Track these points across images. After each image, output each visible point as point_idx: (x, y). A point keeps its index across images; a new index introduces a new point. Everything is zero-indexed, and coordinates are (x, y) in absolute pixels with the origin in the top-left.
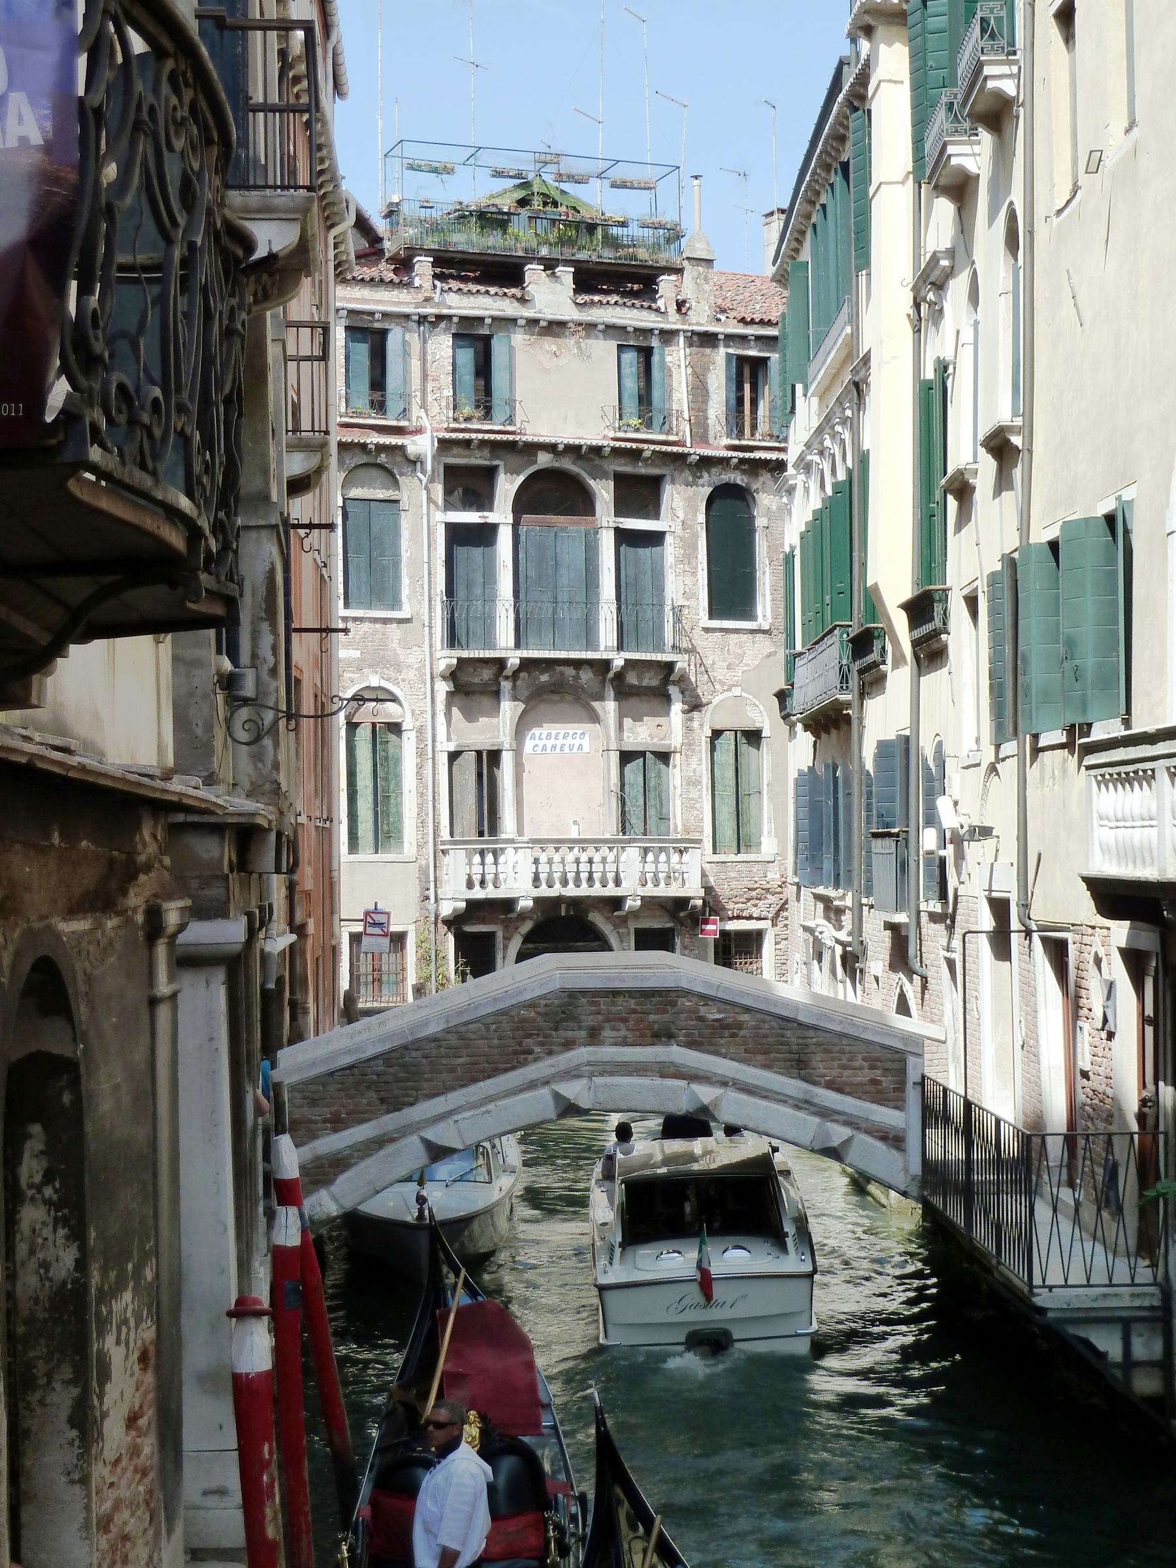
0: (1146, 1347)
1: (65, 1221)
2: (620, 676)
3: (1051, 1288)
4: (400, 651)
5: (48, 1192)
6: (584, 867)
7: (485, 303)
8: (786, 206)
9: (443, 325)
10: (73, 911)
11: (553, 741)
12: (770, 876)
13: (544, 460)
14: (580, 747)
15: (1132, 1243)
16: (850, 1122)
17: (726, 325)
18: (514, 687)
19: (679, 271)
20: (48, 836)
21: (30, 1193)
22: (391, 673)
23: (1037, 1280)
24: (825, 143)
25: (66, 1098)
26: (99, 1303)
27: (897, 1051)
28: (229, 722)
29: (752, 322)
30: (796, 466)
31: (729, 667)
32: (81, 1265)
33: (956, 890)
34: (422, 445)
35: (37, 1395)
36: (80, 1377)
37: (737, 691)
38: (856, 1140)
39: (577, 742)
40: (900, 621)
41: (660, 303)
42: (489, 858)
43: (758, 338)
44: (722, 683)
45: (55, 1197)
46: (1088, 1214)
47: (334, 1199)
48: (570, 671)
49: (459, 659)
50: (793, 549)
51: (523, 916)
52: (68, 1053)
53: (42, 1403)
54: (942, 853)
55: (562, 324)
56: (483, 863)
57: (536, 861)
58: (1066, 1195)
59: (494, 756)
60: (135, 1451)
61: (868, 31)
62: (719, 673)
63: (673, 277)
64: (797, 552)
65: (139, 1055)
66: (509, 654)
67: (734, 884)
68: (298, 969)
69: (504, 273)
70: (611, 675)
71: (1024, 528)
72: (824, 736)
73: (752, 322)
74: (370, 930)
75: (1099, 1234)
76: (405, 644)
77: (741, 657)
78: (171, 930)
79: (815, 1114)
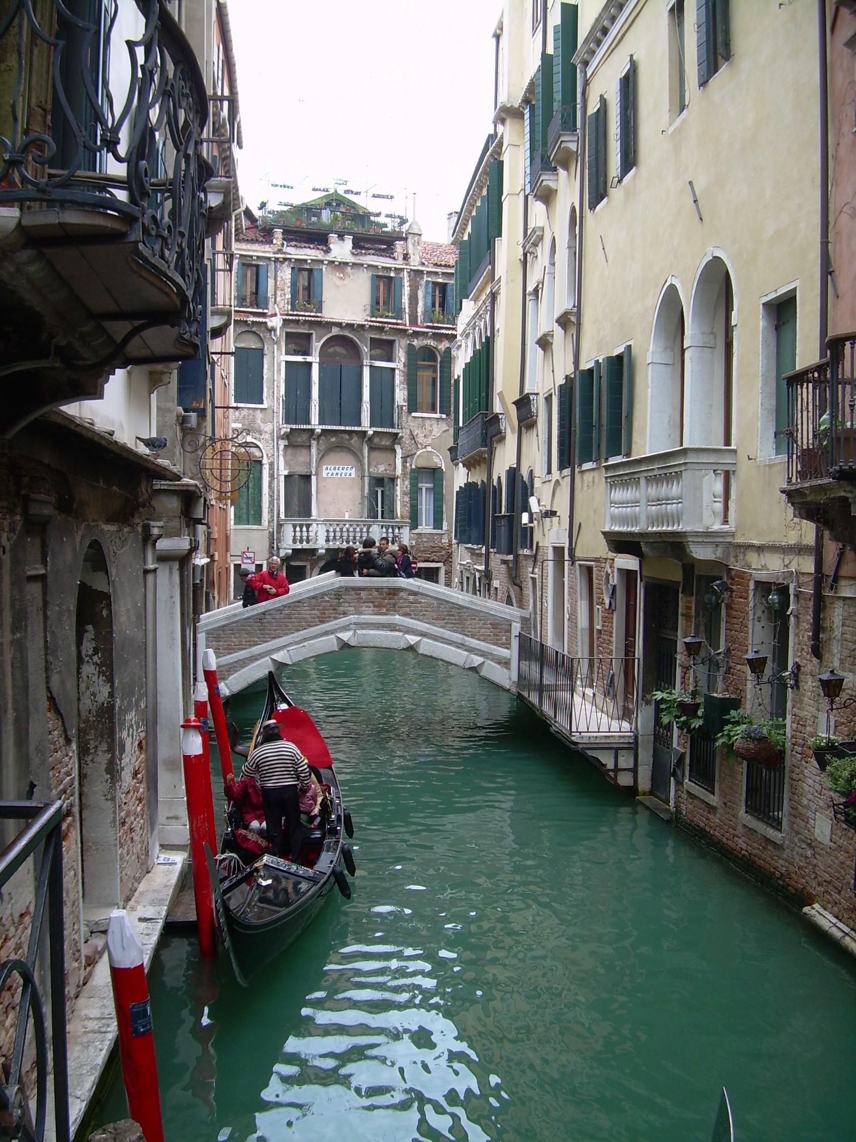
0: (625, 761)
1: (104, 674)
2: (370, 439)
3: (580, 733)
4: (261, 424)
5: (95, 658)
6: (351, 534)
7: (309, 253)
8: (459, 210)
9: (287, 263)
10: (109, 521)
11: (337, 471)
12: (443, 541)
13: (335, 331)
14: (350, 474)
15: (621, 713)
16: (483, 654)
17: (427, 266)
18: (318, 443)
19: (405, 239)
20: (98, 482)
21: (86, 659)
22: (257, 435)
23: (574, 729)
24: (480, 176)
25: (105, 613)
26: (119, 714)
27: (508, 620)
28: (183, 440)
29: (441, 265)
30: (461, 335)
31: (425, 436)
32: (111, 695)
33: (537, 543)
34: (275, 322)
35: (90, 757)
36: (111, 749)
37: (429, 449)
38: (486, 664)
39: (349, 472)
40: (513, 410)
41: (396, 255)
42: (304, 529)
43: (443, 273)
44: (422, 445)
45: (99, 662)
46: (600, 698)
47: (226, 685)
48: (346, 437)
49: (291, 429)
50: (459, 377)
51: (321, 557)
52: (106, 591)
53: (92, 761)
54: (531, 525)
55: (346, 264)
56: (301, 531)
57: (328, 531)
58: (589, 692)
59: (307, 478)
60: (136, 790)
61: (503, 121)
62: (420, 439)
63: (402, 242)
64: (461, 379)
65: (139, 597)
66: (316, 427)
67: (426, 544)
68: (211, 578)
69: (319, 238)
70: (366, 439)
71: (576, 362)
72: (472, 469)
73: (441, 265)
74: (245, 561)
75: (605, 709)
76: (264, 421)
77: (431, 431)
78: (154, 537)
79: (466, 650)
